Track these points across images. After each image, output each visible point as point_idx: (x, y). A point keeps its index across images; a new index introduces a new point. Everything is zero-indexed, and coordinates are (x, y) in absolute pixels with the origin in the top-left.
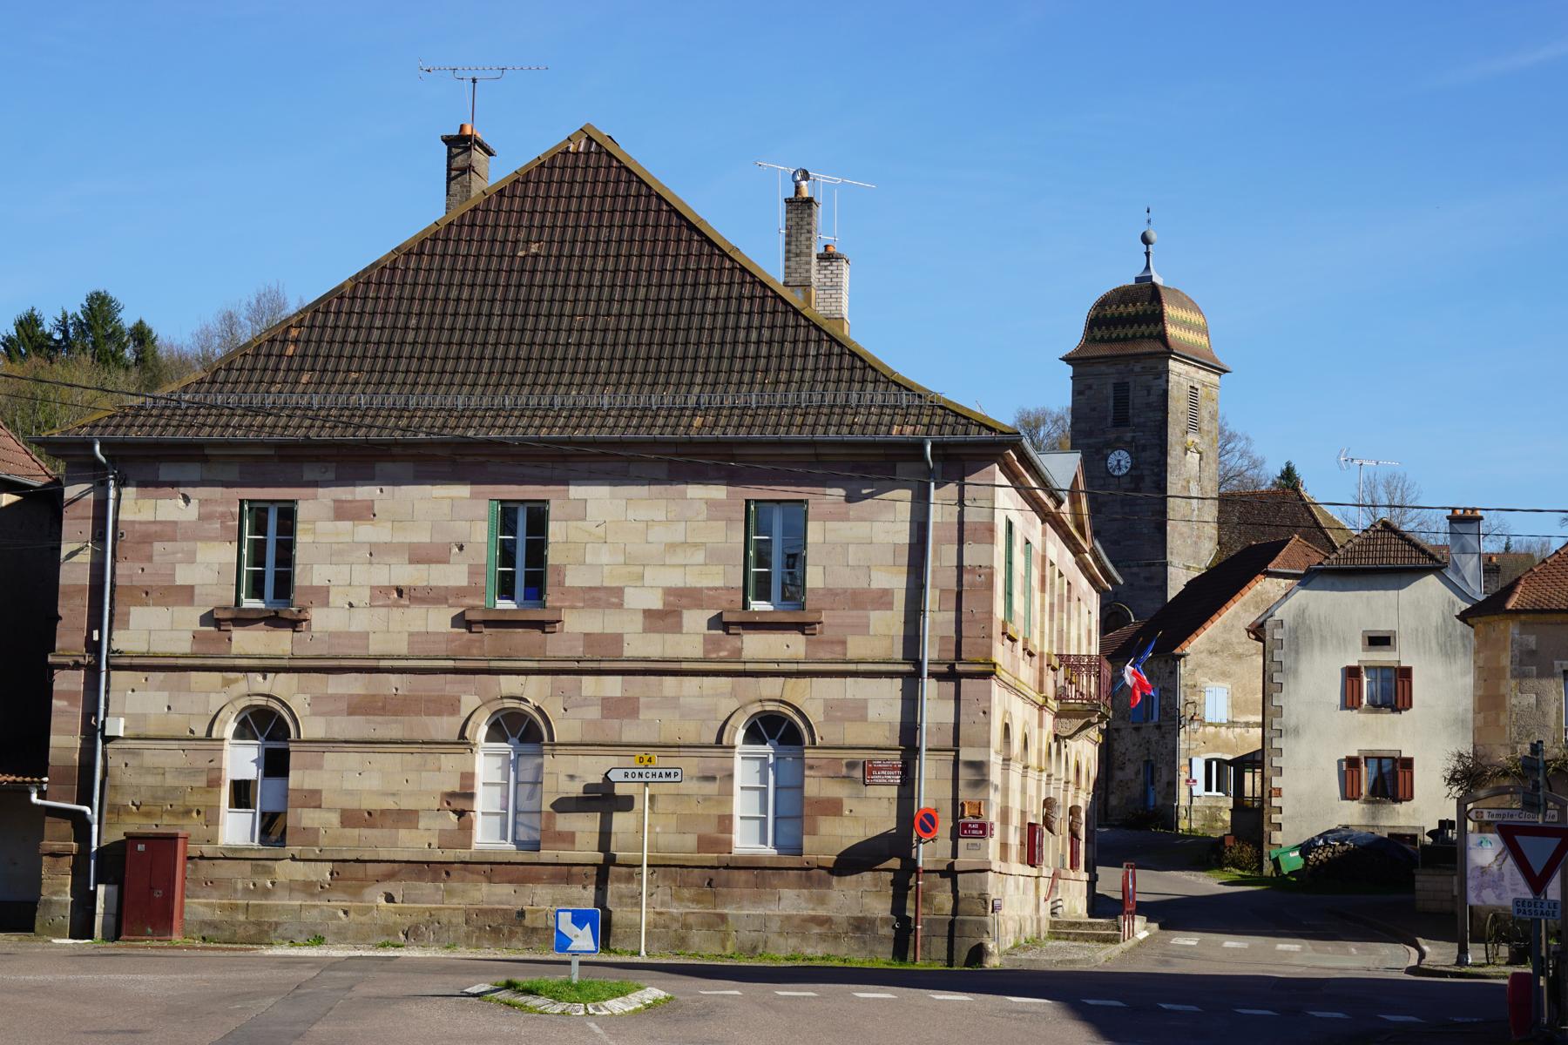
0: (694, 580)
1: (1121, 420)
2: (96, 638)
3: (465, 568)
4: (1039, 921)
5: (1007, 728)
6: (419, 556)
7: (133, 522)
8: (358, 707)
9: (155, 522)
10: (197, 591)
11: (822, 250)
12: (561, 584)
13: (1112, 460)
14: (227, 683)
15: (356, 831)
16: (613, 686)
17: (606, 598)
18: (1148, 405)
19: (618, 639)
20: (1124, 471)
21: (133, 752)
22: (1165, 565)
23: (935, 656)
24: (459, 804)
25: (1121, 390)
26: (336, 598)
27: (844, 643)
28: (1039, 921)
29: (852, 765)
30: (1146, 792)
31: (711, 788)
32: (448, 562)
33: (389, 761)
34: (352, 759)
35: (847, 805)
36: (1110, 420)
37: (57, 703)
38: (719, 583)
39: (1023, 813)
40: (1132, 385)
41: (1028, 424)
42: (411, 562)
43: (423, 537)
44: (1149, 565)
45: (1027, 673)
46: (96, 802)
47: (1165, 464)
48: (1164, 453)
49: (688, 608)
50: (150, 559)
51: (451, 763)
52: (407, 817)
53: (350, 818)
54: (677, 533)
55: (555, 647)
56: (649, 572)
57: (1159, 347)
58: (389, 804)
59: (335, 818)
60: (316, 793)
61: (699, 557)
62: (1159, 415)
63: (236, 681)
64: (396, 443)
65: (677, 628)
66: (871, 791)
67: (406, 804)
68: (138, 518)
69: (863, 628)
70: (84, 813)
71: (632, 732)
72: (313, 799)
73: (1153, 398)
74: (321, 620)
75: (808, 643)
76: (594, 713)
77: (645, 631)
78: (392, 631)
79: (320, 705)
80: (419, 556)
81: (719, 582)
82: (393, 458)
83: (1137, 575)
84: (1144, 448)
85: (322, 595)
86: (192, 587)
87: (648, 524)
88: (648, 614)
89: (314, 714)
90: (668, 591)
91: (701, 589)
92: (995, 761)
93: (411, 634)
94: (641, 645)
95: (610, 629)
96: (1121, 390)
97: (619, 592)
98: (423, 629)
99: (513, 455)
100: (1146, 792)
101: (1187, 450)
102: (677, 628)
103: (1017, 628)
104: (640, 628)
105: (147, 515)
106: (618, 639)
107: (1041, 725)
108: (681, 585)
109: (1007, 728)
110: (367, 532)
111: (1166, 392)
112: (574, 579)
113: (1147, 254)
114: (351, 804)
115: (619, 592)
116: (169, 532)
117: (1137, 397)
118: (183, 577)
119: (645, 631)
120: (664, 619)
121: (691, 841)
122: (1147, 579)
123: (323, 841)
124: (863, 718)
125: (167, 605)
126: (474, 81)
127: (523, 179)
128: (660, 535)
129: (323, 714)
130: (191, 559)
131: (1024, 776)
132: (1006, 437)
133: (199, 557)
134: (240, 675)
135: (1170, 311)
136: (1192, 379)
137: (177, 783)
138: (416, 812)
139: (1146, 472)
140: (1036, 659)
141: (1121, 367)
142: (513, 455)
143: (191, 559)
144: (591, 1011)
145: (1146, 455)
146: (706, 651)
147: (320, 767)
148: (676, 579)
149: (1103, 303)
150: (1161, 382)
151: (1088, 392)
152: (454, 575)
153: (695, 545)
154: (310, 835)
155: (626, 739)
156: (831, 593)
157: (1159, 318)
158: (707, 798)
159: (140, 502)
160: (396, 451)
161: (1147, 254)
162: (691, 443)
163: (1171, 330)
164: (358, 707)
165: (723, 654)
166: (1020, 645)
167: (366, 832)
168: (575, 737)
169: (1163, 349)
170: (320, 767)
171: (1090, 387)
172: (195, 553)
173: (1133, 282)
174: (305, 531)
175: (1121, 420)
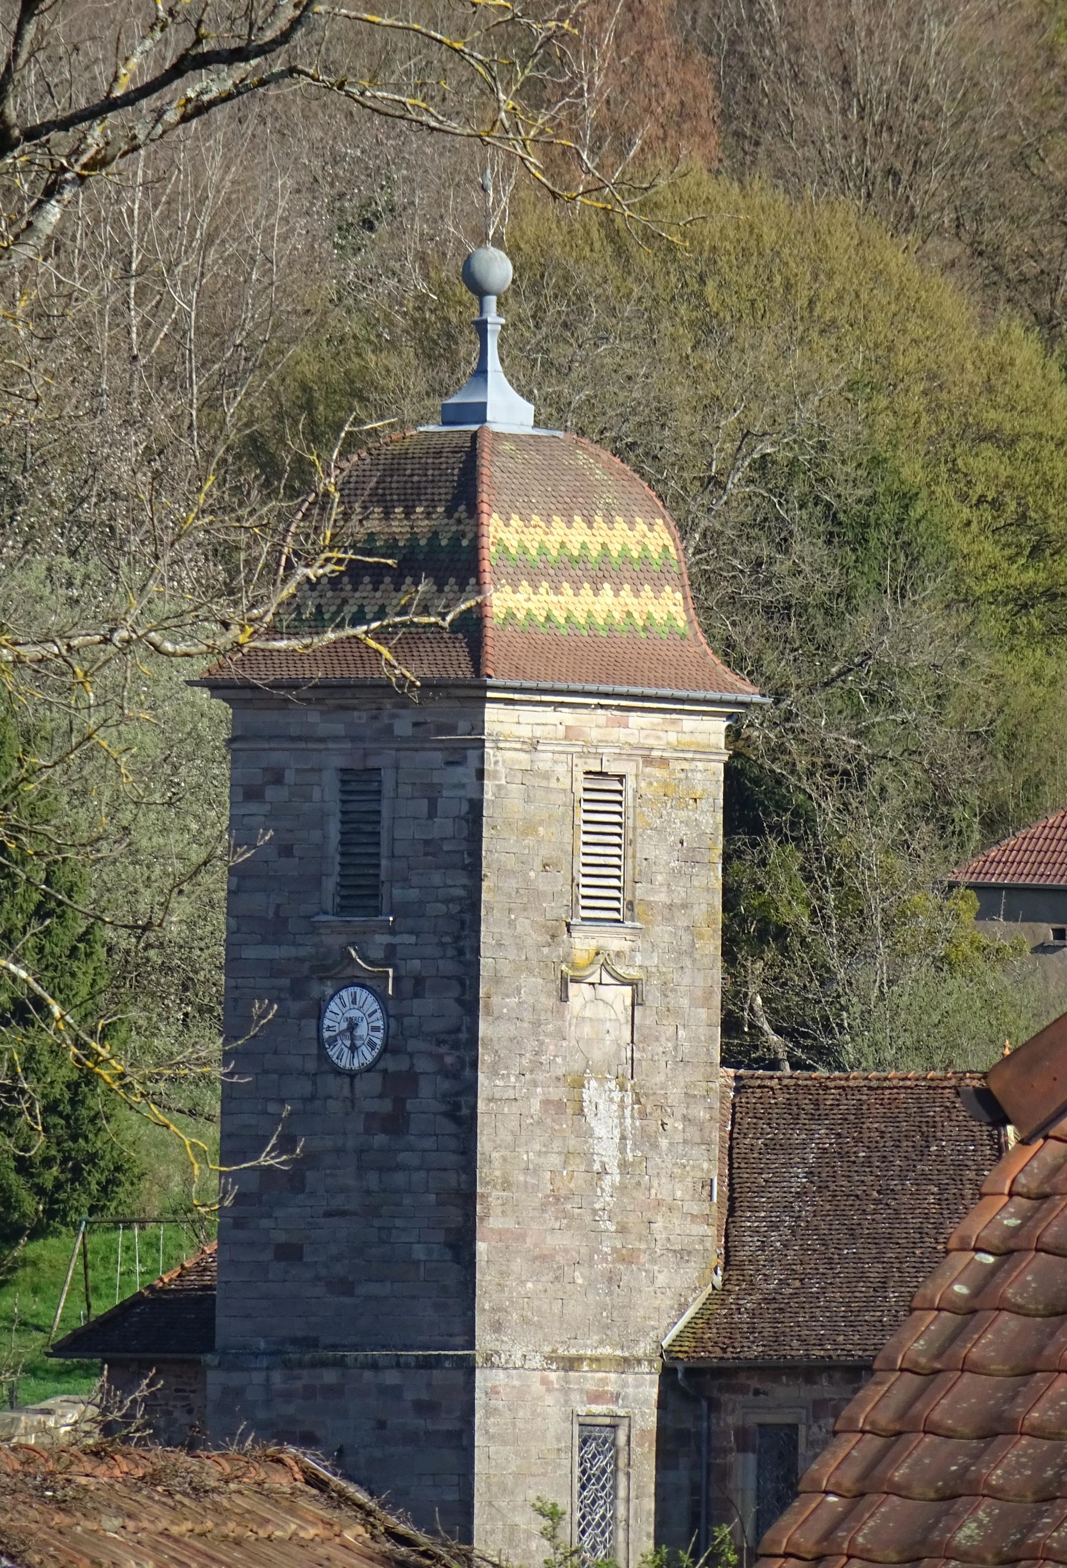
1: (360, 894)
13: (335, 1017)
20: (367, 1056)
22: (468, 1368)
25: (360, 785)
36: (330, 884)
40: (388, 777)
41: (765, 921)
44: (427, 1364)
57: (234, 746)
73: (443, 827)
83: (395, 1392)
96: (360, 785)
111: (476, 807)
117: (402, 822)
122: (423, 1408)
136: (591, 750)
139: (423, 1065)
141: (360, 717)
145: (425, 1006)
150: (463, 774)
151: (270, 793)
163: (654, 538)
169: (465, 672)
171: (277, 778)
174: (704, 751)
175: (360, 894)
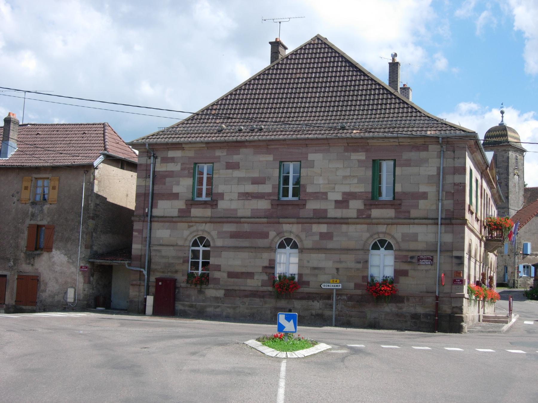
0: (354, 189)
2: (147, 211)
3: (271, 186)
4: (479, 316)
5: (470, 245)
6: (255, 181)
7: (159, 171)
8: (235, 235)
9: (166, 171)
10: (180, 195)
11: (402, 86)
12: (305, 191)
14: (189, 227)
15: (232, 280)
16: (324, 228)
17: (322, 196)
18: (503, 161)
19: (325, 211)
21: (159, 251)
23: (444, 216)
24: (269, 271)
26: (226, 197)
27: (409, 212)
28: (479, 316)
29: (412, 258)
30: (504, 275)
31: (360, 266)
32: (265, 184)
33: (245, 255)
34: (231, 254)
35: (411, 273)
37: (135, 234)
38: (363, 190)
39: (475, 277)
42: (252, 184)
43: (256, 175)
45: (476, 226)
46: (146, 267)
47: (508, 178)
48: (508, 175)
49: (351, 199)
50: (165, 184)
51: (266, 256)
52: (250, 275)
53: (231, 275)
54: (347, 172)
55: (303, 213)
56: (337, 186)
58: (244, 270)
59: (225, 275)
60: (219, 266)
61: (356, 181)
62: (506, 164)
63: (192, 226)
64: (247, 141)
65: (347, 207)
66: (420, 268)
67: (250, 270)
68: (161, 170)
69: (416, 207)
70: (142, 271)
71: (330, 245)
72: (218, 268)
74: (222, 205)
75: (396, 212)
76: (317, 238)
77: (336, 208)
78: (244, 209)
79: (221, 235)
80: (255, 181)
81: (362, 190)
82: (246, 147)
84: (502, 174)
85: (221, 196)
86: (178, 193)
87: (337, 169)
88: (336, 202)
89: (218, 238)
90: (344, 194)
91: (356, 193)
92: (466, 256)
93: (252, 210)
94: (333, 213)
95: (323, 207)
97: (326, 194)
98: (256, 208)
99: (288, 145)
100: (504, 275)
101: (515, 174)
102: (347, 207)
103: (473, 208)
104: (333, 207)
105: (164, 169)
106: (325, 211)
107: (481, 246)
108: (348, 191)
109: (470, 245)
110: (237, 174)
111: (508, 157)
112: (310, 189)
113: (502, 117)
114: (231, 270)
115: (326, 194)
116: (171, 174)
118: (176, 189)
119: (336, 208)
120: (342, 203)
121: (352, 285)
123: (221, 282)
124: (416, 240)
125: (169, 199)
126: (280, 23)
127: (295, 53)
128: (341, 173)
129: (221, 238)
130: (178, 184)
131: (475, 263)
132: (468, 134)
133: (181, 183)
134: (194, 224)
135: (509, 133)
137: (172, 261)
138: (253, 273)
139: (503, 181)
140: (479, 222)
142: (288, 145)
143: (178, 184)
144: (289, 356)
146: (357, 215)
147: (220, 256)
148: (347, 189)
149: (489, 131)
152: (267, 188)
153: (354, 176)
154: (217, 281)
155: (328, 247)
156: (404, 193)
157: (506, 135)
158: (358, 269)
159: (162, 164)
160: (246, 144)
161: (502, 117)
162: (352, 138)
164: (235, 235)
165: (364, 216)
166: (474, 214)
167: (236, 280)
168: (310, 246)
170: (220, 256)
172: (179, 182)
173: (498, 125)
